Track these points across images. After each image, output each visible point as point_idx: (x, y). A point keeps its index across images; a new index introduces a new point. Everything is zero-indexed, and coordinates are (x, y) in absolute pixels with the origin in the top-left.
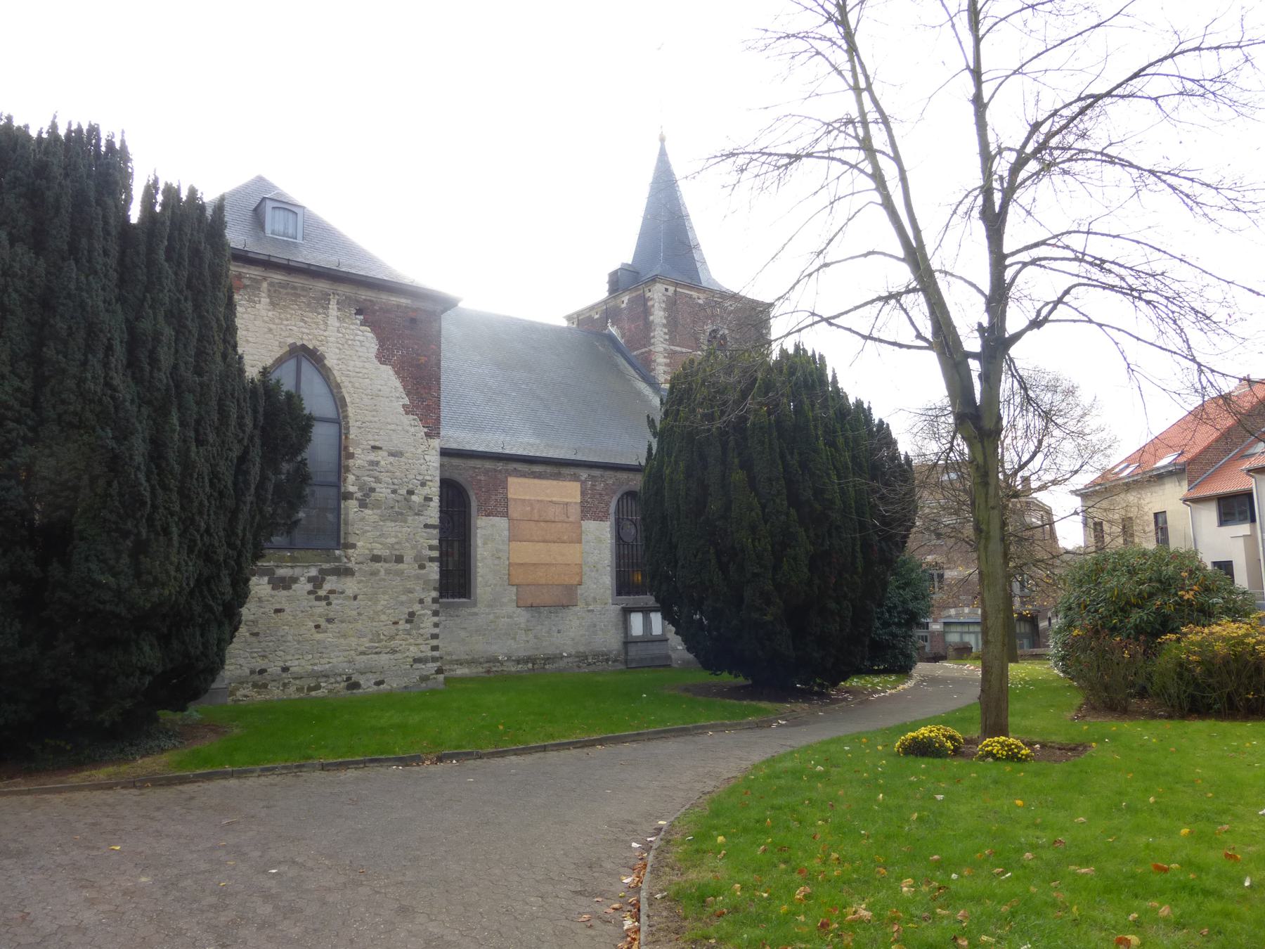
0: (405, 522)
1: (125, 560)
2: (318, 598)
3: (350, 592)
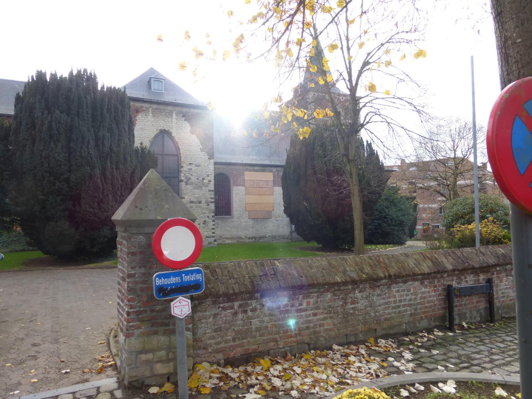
0: (202, 189)
1: (96, 204)
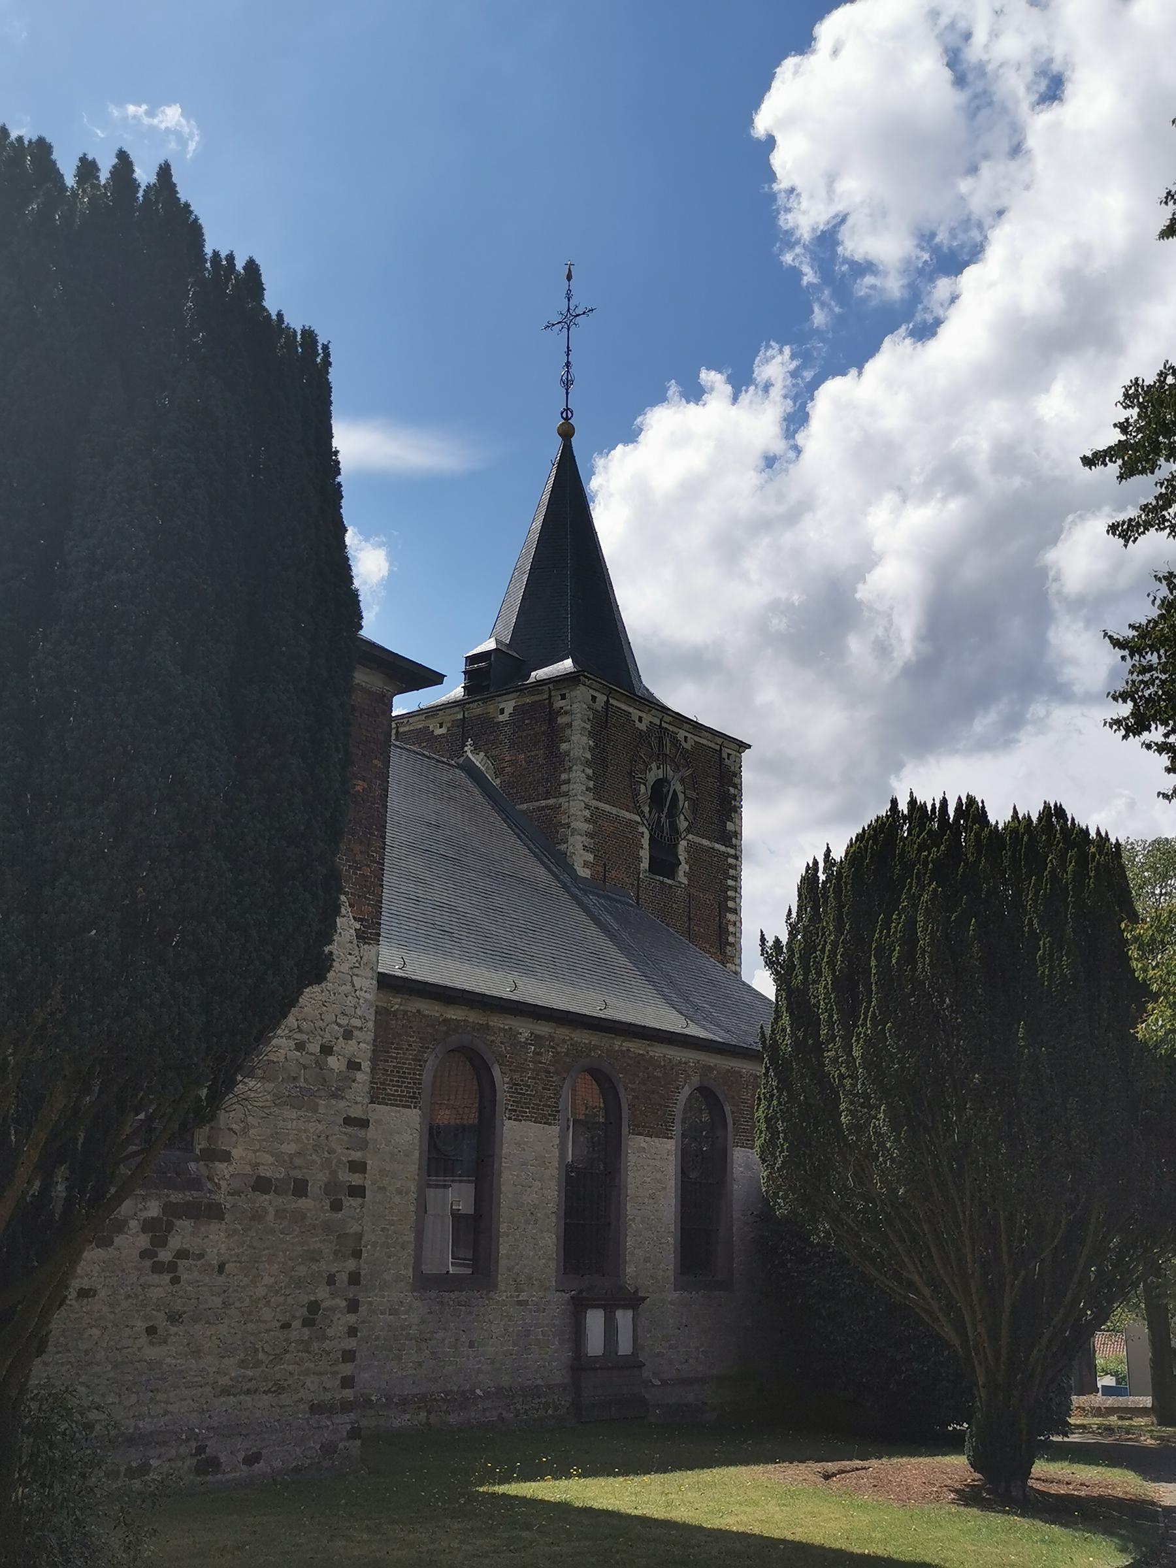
0: (315, 1111)
2: (158, 1268)
3: (213, 1258)
